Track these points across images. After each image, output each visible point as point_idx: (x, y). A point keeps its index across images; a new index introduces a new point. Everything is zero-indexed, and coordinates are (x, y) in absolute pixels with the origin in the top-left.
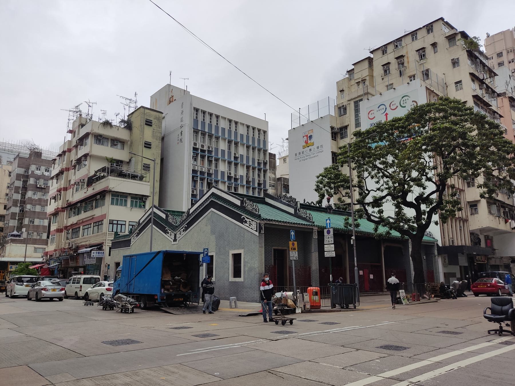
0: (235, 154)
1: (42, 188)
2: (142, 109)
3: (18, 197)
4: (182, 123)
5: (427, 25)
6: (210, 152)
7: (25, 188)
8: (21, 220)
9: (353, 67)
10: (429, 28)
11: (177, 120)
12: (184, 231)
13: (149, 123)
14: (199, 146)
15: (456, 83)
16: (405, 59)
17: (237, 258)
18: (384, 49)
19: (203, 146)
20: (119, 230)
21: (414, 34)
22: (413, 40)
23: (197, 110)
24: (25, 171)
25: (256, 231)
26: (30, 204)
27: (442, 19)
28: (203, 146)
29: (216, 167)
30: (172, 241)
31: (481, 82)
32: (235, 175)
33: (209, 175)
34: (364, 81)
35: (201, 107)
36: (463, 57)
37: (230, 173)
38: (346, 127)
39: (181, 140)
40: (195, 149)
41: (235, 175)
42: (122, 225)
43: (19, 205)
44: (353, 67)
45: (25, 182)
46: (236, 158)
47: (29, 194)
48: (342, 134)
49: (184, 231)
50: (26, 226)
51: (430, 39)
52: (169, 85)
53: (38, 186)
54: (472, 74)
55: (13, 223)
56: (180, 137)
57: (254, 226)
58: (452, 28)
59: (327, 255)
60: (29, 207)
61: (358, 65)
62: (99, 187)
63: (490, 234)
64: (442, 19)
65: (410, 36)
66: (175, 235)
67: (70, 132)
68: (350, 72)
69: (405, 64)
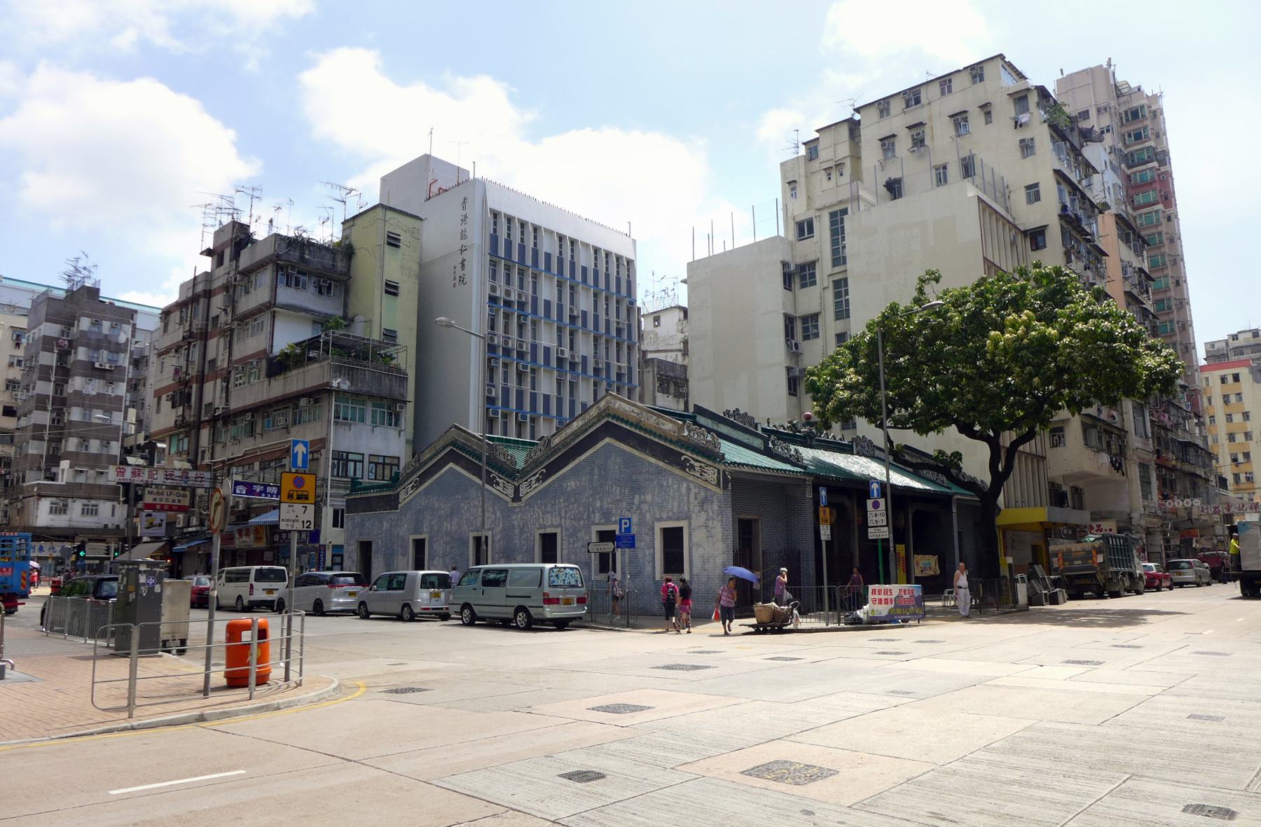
0: (571, 310)
1: (105, 370)
2: (379, 210)
3: (47, 388)
4: (464, 242)
5: (972, 67)
6: (522, 305)
7: (64, 372)
8: (57, 440)
9: (817, 135)
10: (976, 72)
11: (439, 233)
12: (537, 480)
13: (393, 242)
14: (500, 293)
15: (1028, 188)
16: (927, 129)
17: (673, 539)
18: (883, 105)
19: (508, 293)
20: (359, 474)
21: (945, 82)
22: (943, 93)
23: (496, 215)
24: (63, 332)
25: (718, 485)
26: (77, 405)
27: (1001, 57)
28: (508, 293)
29: (534, 337)
30: (508, 499)
31: (1074, 188)
32: (573, 357)
33: (521, 355)
34: (839, 165)
35: (505, 209)
36: (1042, 135)
37: (562, 352)
38: (812, 264)
39: (462, 279)
40: (493, 300)
41: (573, 357)
42: (355, 461)
43: (50, 408)
44: (817, 135)
45: (64, 355)
46: (573, 319)
47: (77, 383)
48: (803, 278)
49: (537, 480)
50: (68, 456)
51: (981, 93)
52: (427, 157)
53: (97, 365)
54: (1058, 173)
55: (36, 449)
56: (459, 272)
57: (711, 474)
58: (1021, 76)
59: (872, 534)
60: (75, 414)
61: (827, 133)
62: (297, 381)
63: (1080, 484)
64: (1001, 57)
65: (937, 84)
66: (517, 490)
67: (208, 252)
68: (812, 146)
69: (927, 142)
